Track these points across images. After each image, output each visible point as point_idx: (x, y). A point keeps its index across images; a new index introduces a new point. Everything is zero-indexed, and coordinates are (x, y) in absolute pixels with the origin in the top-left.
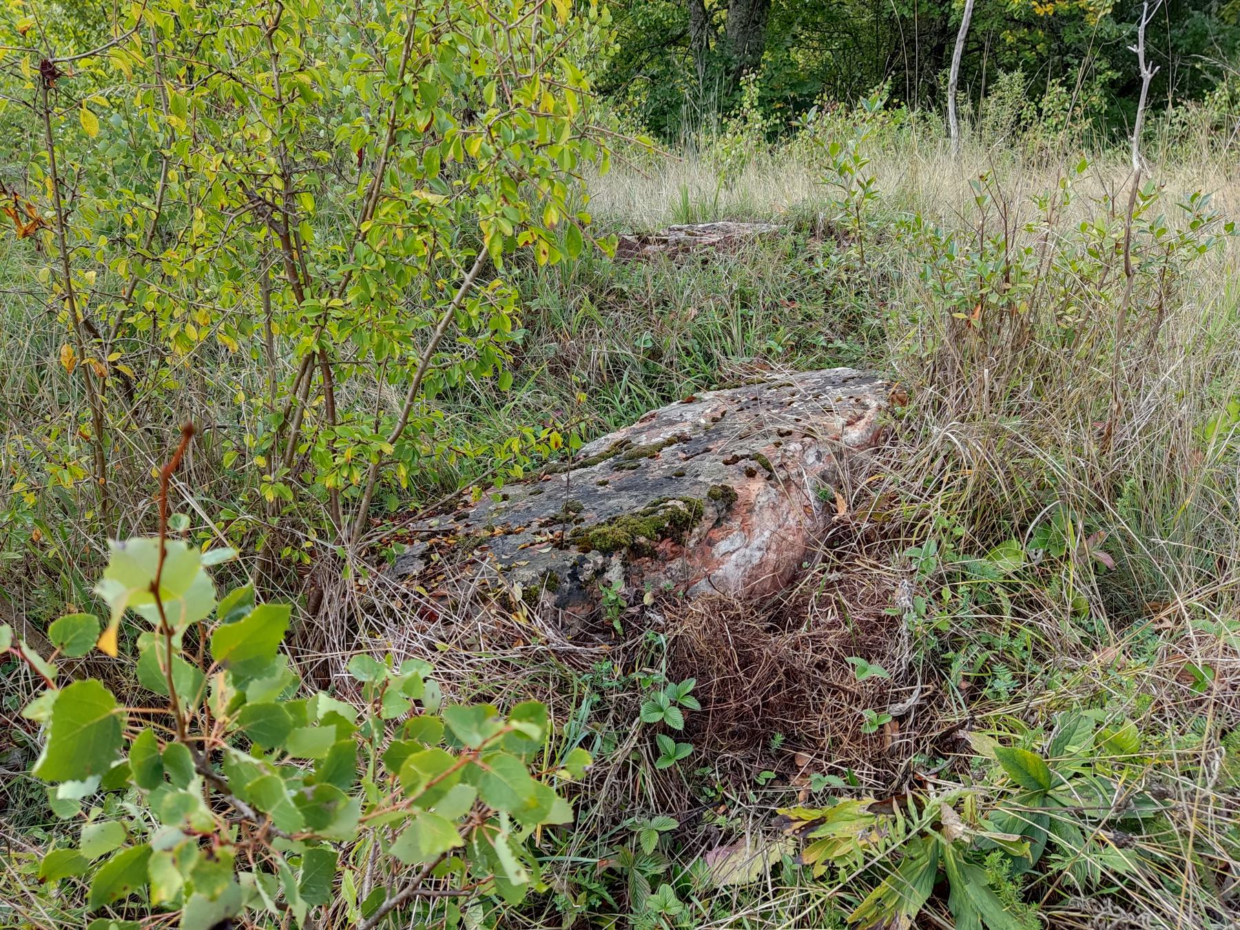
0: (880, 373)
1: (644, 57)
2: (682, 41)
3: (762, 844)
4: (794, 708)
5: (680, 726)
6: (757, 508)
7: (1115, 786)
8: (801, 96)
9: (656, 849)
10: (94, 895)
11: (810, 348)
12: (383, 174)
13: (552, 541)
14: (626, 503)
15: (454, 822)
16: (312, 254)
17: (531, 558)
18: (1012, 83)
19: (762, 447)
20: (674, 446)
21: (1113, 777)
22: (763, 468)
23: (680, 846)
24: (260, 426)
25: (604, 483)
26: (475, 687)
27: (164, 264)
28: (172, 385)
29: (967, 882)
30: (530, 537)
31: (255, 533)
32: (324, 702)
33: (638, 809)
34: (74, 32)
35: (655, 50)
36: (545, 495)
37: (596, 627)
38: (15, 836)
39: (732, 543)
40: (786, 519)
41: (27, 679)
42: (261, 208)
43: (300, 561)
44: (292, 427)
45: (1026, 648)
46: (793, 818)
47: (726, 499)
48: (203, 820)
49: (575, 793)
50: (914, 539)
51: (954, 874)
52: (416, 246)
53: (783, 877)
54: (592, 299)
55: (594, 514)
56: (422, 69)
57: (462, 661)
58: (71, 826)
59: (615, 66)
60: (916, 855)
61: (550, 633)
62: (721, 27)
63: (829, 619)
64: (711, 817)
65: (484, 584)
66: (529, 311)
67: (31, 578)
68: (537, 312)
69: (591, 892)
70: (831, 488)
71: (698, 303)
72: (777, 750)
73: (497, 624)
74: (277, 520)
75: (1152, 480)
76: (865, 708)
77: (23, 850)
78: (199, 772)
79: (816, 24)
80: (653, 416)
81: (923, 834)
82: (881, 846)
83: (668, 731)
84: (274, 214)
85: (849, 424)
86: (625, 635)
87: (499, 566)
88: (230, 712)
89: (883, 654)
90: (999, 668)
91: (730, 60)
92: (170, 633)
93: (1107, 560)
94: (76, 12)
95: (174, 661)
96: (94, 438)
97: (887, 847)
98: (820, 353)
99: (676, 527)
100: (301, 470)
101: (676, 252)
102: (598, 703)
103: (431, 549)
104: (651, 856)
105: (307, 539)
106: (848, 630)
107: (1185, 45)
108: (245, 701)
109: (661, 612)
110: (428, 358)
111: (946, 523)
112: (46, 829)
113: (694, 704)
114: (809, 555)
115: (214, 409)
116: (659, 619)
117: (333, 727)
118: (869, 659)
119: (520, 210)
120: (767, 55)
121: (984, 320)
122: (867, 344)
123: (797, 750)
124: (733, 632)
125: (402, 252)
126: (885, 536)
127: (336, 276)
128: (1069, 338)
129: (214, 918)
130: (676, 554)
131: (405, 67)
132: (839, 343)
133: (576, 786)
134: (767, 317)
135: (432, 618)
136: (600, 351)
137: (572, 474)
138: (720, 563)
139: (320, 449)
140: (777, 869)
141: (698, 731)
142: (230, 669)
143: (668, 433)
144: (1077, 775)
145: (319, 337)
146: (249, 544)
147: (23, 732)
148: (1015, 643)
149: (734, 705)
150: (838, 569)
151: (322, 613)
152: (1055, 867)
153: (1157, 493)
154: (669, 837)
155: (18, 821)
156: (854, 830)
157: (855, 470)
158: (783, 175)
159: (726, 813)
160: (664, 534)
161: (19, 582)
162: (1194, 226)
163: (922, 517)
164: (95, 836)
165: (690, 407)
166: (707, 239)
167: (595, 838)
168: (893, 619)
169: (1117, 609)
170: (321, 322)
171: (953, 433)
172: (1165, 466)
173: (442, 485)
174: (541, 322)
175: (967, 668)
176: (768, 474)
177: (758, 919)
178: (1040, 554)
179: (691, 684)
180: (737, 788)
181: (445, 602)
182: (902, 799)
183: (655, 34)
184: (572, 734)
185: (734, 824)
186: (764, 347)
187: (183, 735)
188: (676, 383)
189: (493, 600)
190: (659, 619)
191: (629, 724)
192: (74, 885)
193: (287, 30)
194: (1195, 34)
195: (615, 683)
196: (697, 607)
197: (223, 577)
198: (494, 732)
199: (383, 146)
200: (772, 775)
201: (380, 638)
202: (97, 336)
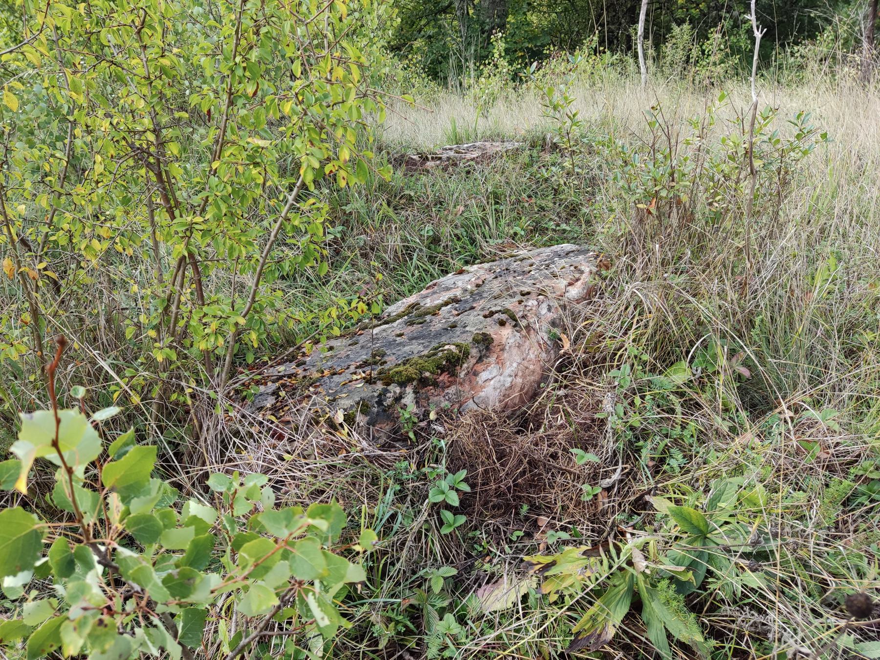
1: (423, 22)
2: (449, 10)
3: (515, 581)
4: (536, 486)
6: (507, 348)
7: (750, 529)
8: (536, 46)
9: (443, 589)
11: (544, 231)
12: (225, 127)
13: (364, 378)
14: (417, 349)
16: (180, 185)
17: (350, 392)
18: (682, 33)
19: (510, 304)
20: (449, 306)
21: (750, 523)
22: (511, 319)
25: (400, 335)
28: (88, 280)
30: (349, 377)
33: (429, 563)
34: (7, 22)
35: (430, 17)
36: (359, 345)
37: (397, 438)
40: (528, 354)
44: (173, 308)
45: (692, 436)
46: (535, 562)
47: (485, 342)
50: (615, 363)
51: (645, 595)
53: (529, 604)
55: (393, 357)
59: (402, 30)
60: (617, 583)
61: (364, 444)
63: (559, 422)
64: (480, 565)
65: (317, 412)
66: (345, 213)
68: (351, 213)
69: (398, 622)
71: (464, 201)
73: (326, 439)
75: (776, 315)
76: (584, 483)
78: (99, 562)
80: (435, 285)
81: (621, 569)
82: (593, 579)
83: (449, 507)
84: (149, 158)
85: (570, 284)
86: (417, 442)
87: (327, 398)
88: (121, 520)
89: (596, 445)
91: (484, 23)
93: (746, 373)
94: (7, 7)
97: (597, 579)
98: (550, 234)
99: (452, 365)
100: (182, 338)
101: (447, 166)
102: (400, 491)
104: (439, 594)
108: (130, 514)
109: (442, 425)
110: (266, 255)
111: (636, 352)
114: (544, 378)
116: (440, 429)
120: (510, 19)
122: (584, 226)
123: (539, 515)
124: (491, 435)
126: (596, 362)
127: (197, 200)
128: (717, 218)
130: (451, 383)
131: (236, 51)
132: (564, 226)
134: (512, 210)
135: (281, 437)
136: (394, 241)
138: (482, 387)
139: (193, 323)
140: (525, 598)
141: (470, 506)
142: (118, 492)
143: (445, 296)
144: (727, 523)
145: (188, 244)
148: (686, 433)
149: (494, 487)
150: (566, 387)
152: (712, 587)
153: (780, 321)
154: (452, 581)
156: (575, 569)
157: (575, 318)
158: (524, 105)
159: (490, 561)
160: (443, 370)
162: (798, 137)
163: (621, 348)
165: (461, 277)
166: (469, 156)
167: (400, 585)
168: (602, 421)
170: (188, 234)
171: (638, 289)
173: (287, 341)
174: (353, 222)
175: (653, 452)
177: (513, 634)
178: (699, 370)
179: (463, 474)
180: (498, 544)
181: (289, 426)
185: (496, 568)
186: (512, 232)
188: (451, 261)
189: (322, 422)
190: (440, 429)
191: (422, 504)
193: (151, 27)
195: (411, 476)
196: (467, 420)
200: (521, 534)
202: (30, 250)
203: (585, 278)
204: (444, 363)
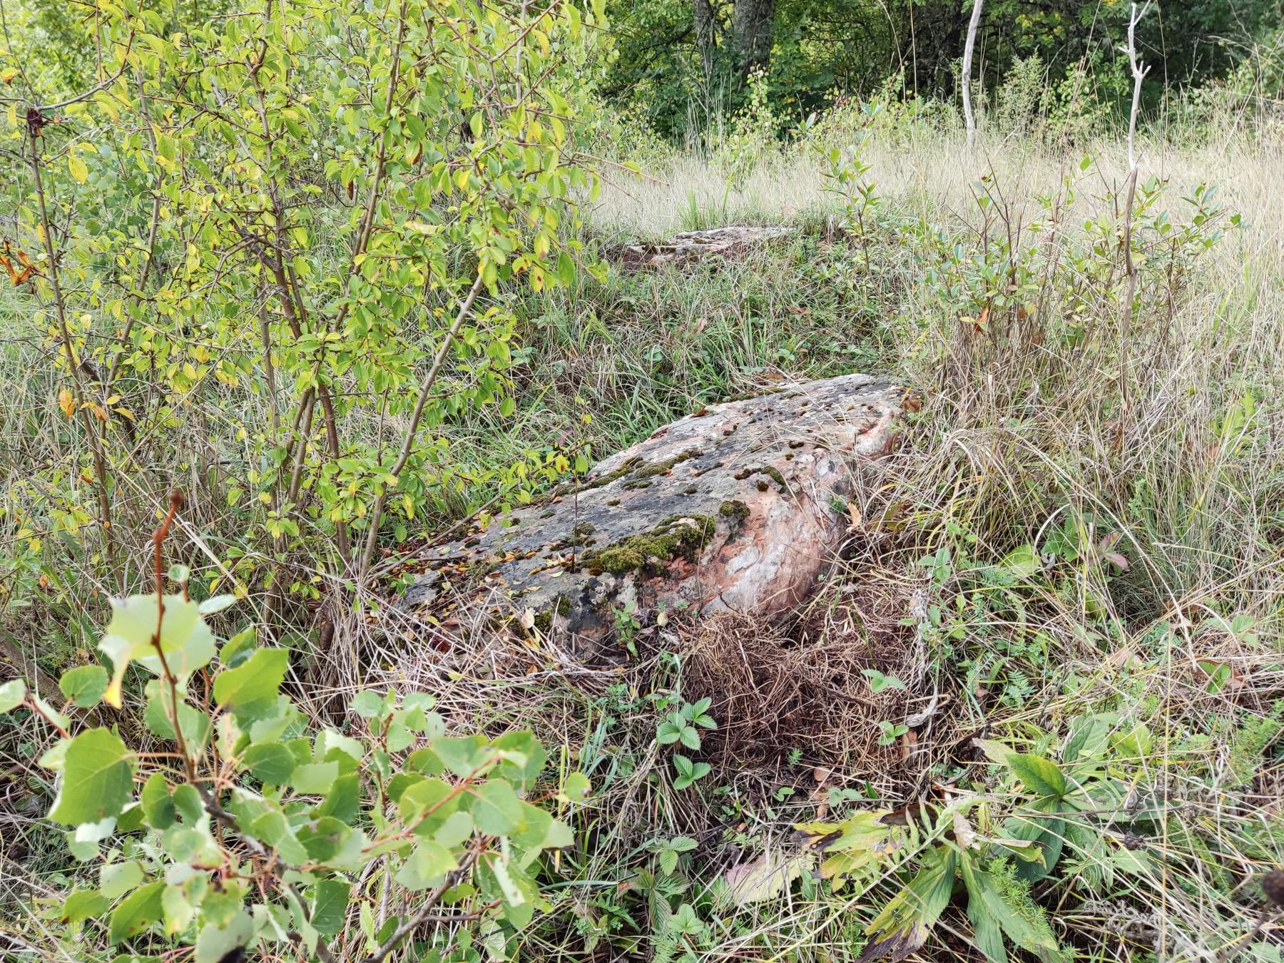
0: (894, 379)
1: (649, 55)
3: (782, 859)
5: (696, 746)
6: (770, 523)
7: (1127, 789)
8: (812, 89)
9: (676, 870)
10: (114, 932)
11: (823, 355)
12: (374, 206)
13: (564, 564)
14: (638, 523)
15: (453, 850)
17: (543, 583)
18: (1027, 70)
19: (775, 460)
20: (686, 462)
21: (1126, 779)
23: (700, 865)
24: (264, 462)
25: (615, 503)
26: (491, 715)
27: (160, 304)
28: (173, 422)
29: (984, 890)
30: (542, 562)
31: (262, 570)
32: (331, 737)
33: (657, 831)
34: (59, 56)
35: (660, 48)
36: (555, 518)
37: (610, 650)
38: (36, 883)
39: (745, 559)
41: (40, 725)
42: (254, 245)
43: (309, 596)
44: (295, 462)
45: (1042, 653)
46: (811, 832)
47: (738, 514)
48: (211, 855)
49: (593, 817)
50: (928, 547)
51: (972, 883)
52: (413, 276)
53: (802, 893)
54: (599, 316)
55: (605, 535)
56: (408, 102)
57: (476, 689)
58: (92, 871)
59: (619, 66)
60: (931, 865)
61: (564, 658)
62: (728, 23)
63: (846, 632)
64: (731, 836)
65: (496, 611)
66: (536, 328)
67: (40, 624)
68: (544, 329)
69: (612, 916)
70: (843, 499)
71: (706, 310)
72: (796, 766)
73: (510, 651)
74: (284, 556)
76: (882, 720)
77: (45, 896)
79: (825, 15)
80: (664, 432)
81: (937, 843)
83: (685, 751)
84: (267, 250)
85: (862, 432)
87: (511, 593)
88: (237, 752)
90: (1015, 674)
91: (737, 55)
92: (173, 681)
93: (1121, 562)
94: (59, 35)
95: (178, 706)
96: (97, 480)
97: (902, 858)
98: (833, 359)
100: (306, 505)
102: (615, 726)
103: (442, 577)
104: (671, 877)
105: (316, 574)
106: (864, 642)
107: (1207, 21)
109: (675, 632)
110: (428, 388)
111: (959, 531)
112: (67, 874)
113: (710, 723)
114: (824, 568)
115: (216, 443)
116: (672, 638)
117: (336, 763)
118: (885, 671)
119: (514, 239)
120: (776, 50)
121: (991, 323)
123: (816, 765)
124: (747, 649)
125: (397, 283)
126: (900, 545)
127: (332, 308)
128: (1078, 337)
129: (226, 946)
130: (689, 573)
131: (391, 99)
132: (852, 348)
133: (595, 811)
134: (778, 325)
135: (444, 648)
136: (607, 369)
137: (581, 496)
138: (733, 580)
139: (324, 482)
140: (796, 884)
142: (234, 712)
143: (679, 449)
144: (1092, 779)
145: (318, 371)
146: (259, 580)
147: (39, 779)
148: (1032, 648)
149: (751, 723)
150: (855, 580)
151: (334, 648)
154: (690, 857)
155: (38, 867)
156: (869, 842)
158: (794, 173)
159: (746, 830)
161: (28, 629)
162: (1197, 220)
163: (936, 524)
164: (116, 879)
165: (702, 420)
166: (714, 247)
167: (615, 862)
168: (909, 629)
169: (1137, 610)
170: (319, 356)
171: (961, 440)
172: (1178, 465)
173: (453, 511)
174: (547, 340)
175: (983, 676)
176: (780, 487)
177: (779, 935)
179: (706, 703)
180: (757, 805)
181: (457, 632)
182: (915, 807)
183: (660, 32)
184: (588, 758)
185: (753, 841)
186: (776, 356)
187: (192, 776)
189: (505, 627)
190: (672, 638)
191: (646, 746)
192: (97, 928)
193: (273, 66)
194: (1217, 10)
195: (630, 706)
196: (711, 626)
197: (224, 624)
198: (486, 760)
199: (373, 180)
200: (791, 791)
201: (393, 669)
203: (884, 422)
204: (678, 544)
